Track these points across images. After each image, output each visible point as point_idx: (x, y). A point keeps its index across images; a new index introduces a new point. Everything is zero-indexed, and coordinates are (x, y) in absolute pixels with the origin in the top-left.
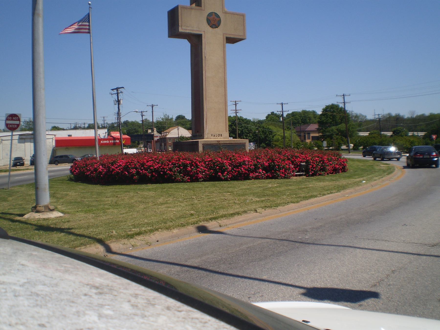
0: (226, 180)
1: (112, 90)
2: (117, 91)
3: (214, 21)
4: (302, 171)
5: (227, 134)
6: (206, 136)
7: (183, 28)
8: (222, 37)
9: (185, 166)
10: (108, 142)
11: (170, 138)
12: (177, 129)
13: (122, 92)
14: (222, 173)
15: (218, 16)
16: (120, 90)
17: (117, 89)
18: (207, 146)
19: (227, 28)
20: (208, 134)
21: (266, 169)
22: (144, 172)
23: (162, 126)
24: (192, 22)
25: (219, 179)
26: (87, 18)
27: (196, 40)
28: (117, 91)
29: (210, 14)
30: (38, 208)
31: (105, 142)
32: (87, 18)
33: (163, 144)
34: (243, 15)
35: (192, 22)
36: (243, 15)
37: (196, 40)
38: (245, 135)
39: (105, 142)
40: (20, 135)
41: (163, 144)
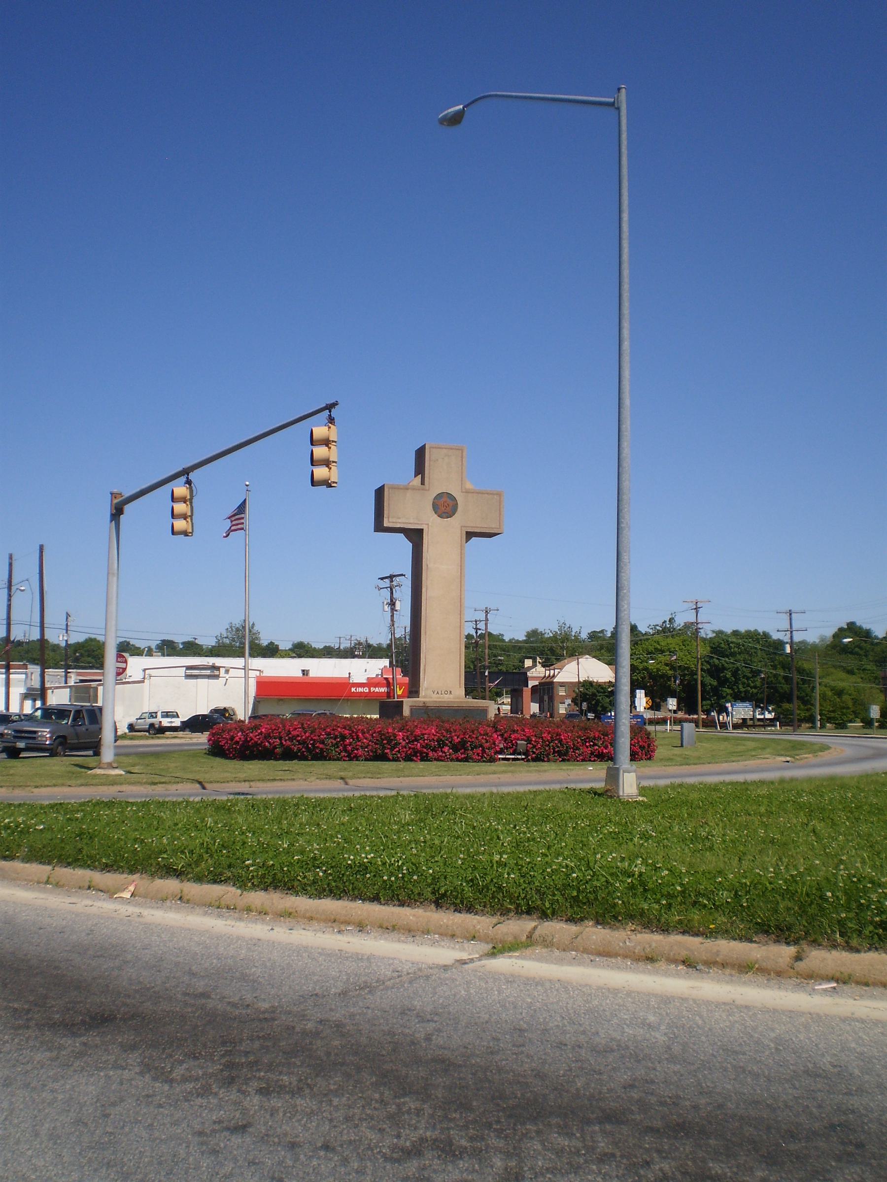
0: (396, 760)
1: (382, 579)
2: (392, 581)
3: (445, 506)
4: (519, 754)
5: (462, 692)
6: (422, 693)
7: (391, 520)
8: (459, 531)
9: (343, 737)
10: (366, 690)
11: (562, 684)
12: (574, 663)
13: (399, 586)
14: (392, 749)
15: (454, 499)
16: (398, 579)
17: (391, 577)
18: (426, 710)
19: (468, 515)
20: (427, 689)
21: (455, 748)
22: (289, 743)
23: (554, 648)
24: (407, 510)
25: (383, 758)
26: (242, 508)
27: (415, 536)
28: (392, 581)
29: (440, 496)
30: (102, 765)
31: (360, 690)
32: (242, 508)
33: (546, 698)
34: (499, 494)
35: (407, 510)
36: (499, 494)
37: (415, 536)
38: (743, 683)
39: (360, 690)
40: (189, 668)
41: (546, 698)
